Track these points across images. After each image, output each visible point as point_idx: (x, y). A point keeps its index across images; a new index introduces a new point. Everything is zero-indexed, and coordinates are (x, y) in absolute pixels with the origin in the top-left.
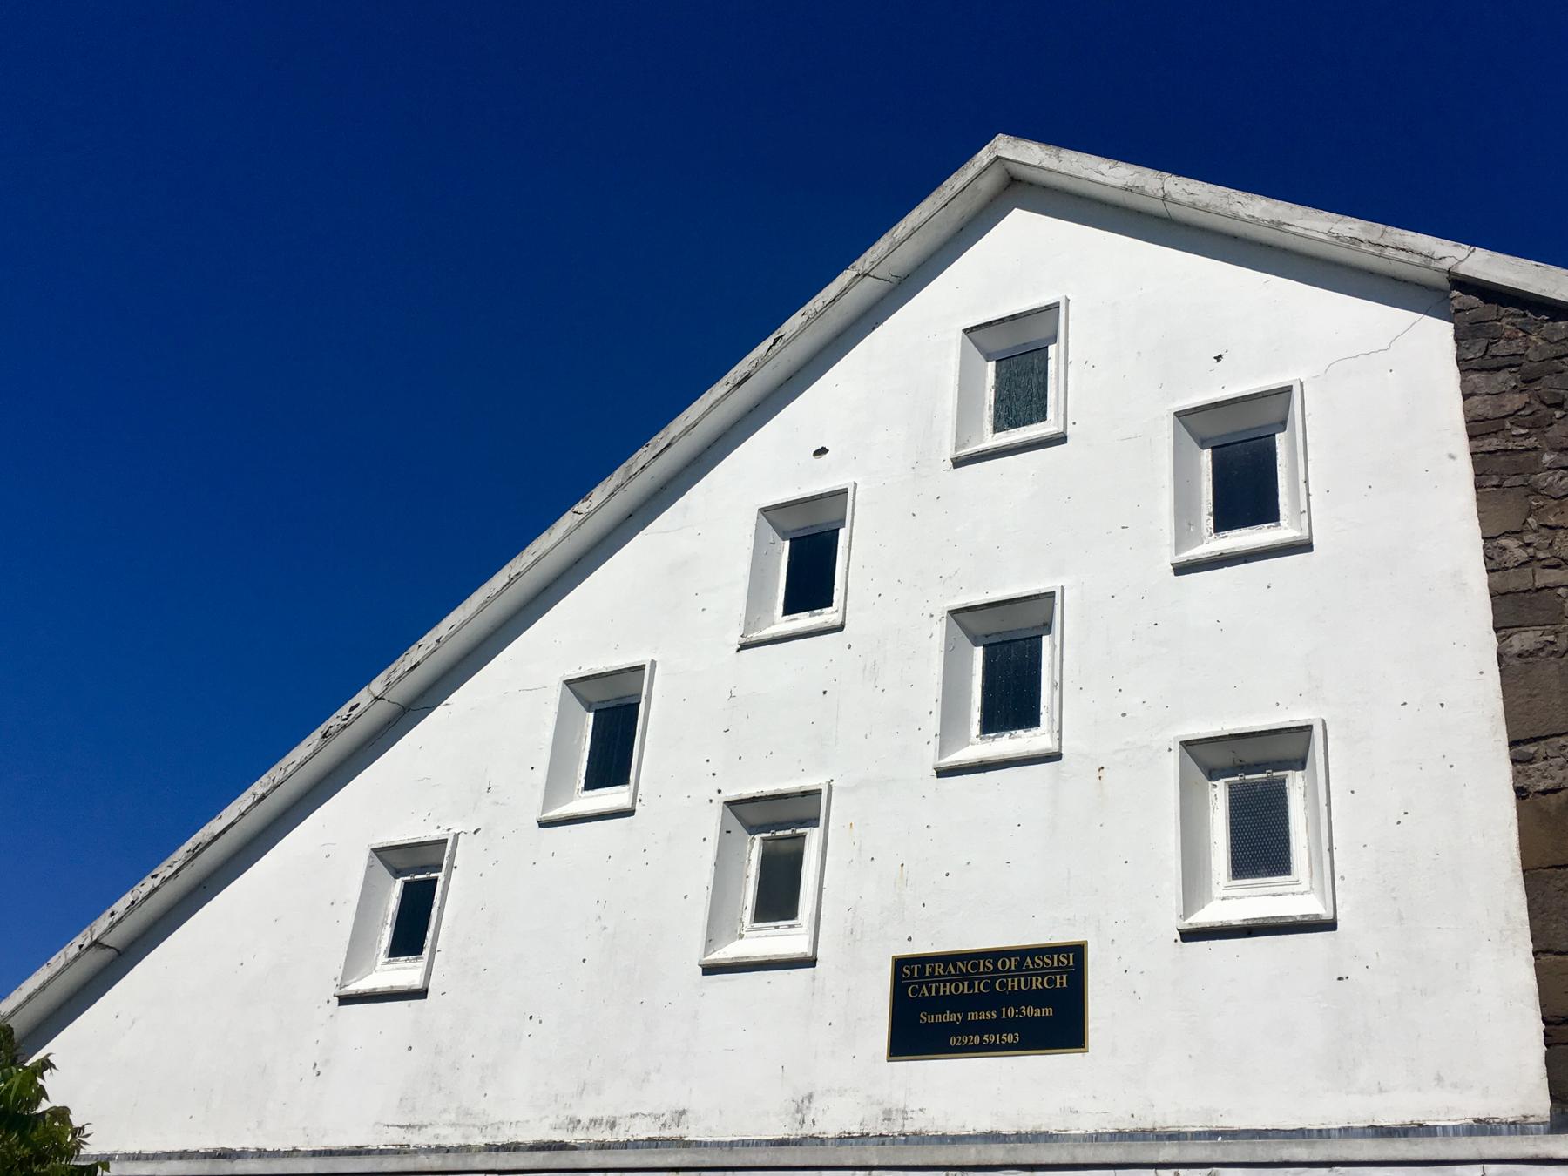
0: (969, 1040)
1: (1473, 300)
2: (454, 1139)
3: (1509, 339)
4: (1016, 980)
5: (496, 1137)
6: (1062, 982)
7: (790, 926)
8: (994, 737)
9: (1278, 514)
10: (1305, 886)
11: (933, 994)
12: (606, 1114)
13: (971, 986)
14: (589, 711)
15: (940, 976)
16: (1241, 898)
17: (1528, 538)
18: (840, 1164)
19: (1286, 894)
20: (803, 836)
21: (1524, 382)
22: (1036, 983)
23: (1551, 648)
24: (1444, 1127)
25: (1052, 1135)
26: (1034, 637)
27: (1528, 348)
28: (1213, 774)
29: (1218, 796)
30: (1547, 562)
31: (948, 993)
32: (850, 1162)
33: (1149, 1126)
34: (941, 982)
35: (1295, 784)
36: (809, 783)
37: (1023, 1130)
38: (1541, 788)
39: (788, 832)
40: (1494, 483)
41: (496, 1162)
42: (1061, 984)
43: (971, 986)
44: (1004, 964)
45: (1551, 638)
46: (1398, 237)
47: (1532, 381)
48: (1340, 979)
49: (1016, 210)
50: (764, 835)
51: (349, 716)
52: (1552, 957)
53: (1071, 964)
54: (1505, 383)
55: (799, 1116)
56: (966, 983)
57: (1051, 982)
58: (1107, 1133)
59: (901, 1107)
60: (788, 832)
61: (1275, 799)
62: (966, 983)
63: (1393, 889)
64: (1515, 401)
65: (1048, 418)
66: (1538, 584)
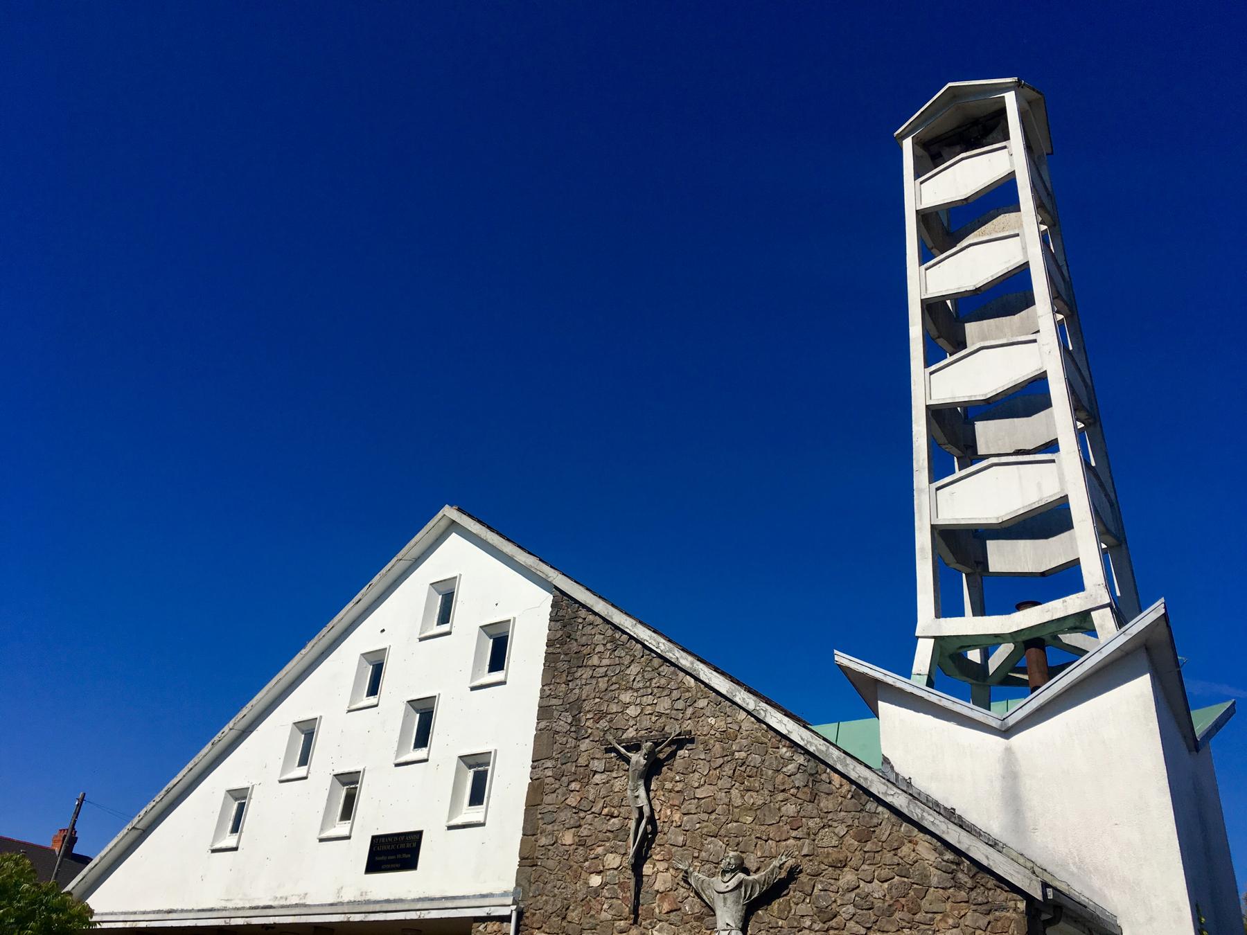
6: (414, 845)
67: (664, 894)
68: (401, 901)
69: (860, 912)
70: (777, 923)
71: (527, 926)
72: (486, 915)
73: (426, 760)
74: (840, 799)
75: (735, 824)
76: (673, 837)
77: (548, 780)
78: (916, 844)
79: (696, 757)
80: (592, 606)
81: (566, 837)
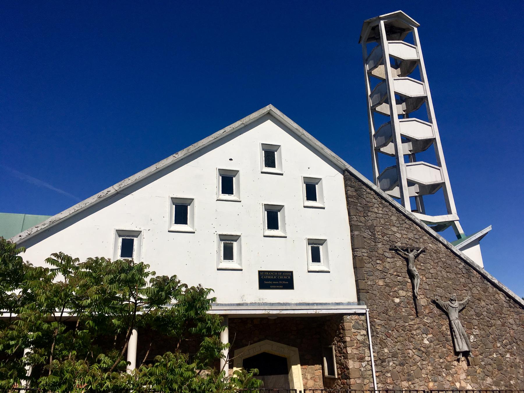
1: (349, 174)
3: (353, 183)
6: (289, 277)
7: (232, 261)
10: (323, 265)
13: (273, 277)
17: (357, 217)
20: (233, 243)
22: (285, 277)
33: (304, 302)
35: (235, 245)
43: (273, 277)
44: (279, 274)
49: (269, 120)
50: (224, 242)
51: (107, 194)
52: (360, 280)
59: (262, 298)
61: (318, 249)
64: (355, 194)
66: (358, 225)
67: (425, 307)
68: (289, 304)
69: (488, 314)
70: (465, 317)
72: (353, 312)
74: (477, 279)
75: (446, 284)
76: (425, 286)
78: (499, 294)
79: (428, 258)
81: (380, 282)
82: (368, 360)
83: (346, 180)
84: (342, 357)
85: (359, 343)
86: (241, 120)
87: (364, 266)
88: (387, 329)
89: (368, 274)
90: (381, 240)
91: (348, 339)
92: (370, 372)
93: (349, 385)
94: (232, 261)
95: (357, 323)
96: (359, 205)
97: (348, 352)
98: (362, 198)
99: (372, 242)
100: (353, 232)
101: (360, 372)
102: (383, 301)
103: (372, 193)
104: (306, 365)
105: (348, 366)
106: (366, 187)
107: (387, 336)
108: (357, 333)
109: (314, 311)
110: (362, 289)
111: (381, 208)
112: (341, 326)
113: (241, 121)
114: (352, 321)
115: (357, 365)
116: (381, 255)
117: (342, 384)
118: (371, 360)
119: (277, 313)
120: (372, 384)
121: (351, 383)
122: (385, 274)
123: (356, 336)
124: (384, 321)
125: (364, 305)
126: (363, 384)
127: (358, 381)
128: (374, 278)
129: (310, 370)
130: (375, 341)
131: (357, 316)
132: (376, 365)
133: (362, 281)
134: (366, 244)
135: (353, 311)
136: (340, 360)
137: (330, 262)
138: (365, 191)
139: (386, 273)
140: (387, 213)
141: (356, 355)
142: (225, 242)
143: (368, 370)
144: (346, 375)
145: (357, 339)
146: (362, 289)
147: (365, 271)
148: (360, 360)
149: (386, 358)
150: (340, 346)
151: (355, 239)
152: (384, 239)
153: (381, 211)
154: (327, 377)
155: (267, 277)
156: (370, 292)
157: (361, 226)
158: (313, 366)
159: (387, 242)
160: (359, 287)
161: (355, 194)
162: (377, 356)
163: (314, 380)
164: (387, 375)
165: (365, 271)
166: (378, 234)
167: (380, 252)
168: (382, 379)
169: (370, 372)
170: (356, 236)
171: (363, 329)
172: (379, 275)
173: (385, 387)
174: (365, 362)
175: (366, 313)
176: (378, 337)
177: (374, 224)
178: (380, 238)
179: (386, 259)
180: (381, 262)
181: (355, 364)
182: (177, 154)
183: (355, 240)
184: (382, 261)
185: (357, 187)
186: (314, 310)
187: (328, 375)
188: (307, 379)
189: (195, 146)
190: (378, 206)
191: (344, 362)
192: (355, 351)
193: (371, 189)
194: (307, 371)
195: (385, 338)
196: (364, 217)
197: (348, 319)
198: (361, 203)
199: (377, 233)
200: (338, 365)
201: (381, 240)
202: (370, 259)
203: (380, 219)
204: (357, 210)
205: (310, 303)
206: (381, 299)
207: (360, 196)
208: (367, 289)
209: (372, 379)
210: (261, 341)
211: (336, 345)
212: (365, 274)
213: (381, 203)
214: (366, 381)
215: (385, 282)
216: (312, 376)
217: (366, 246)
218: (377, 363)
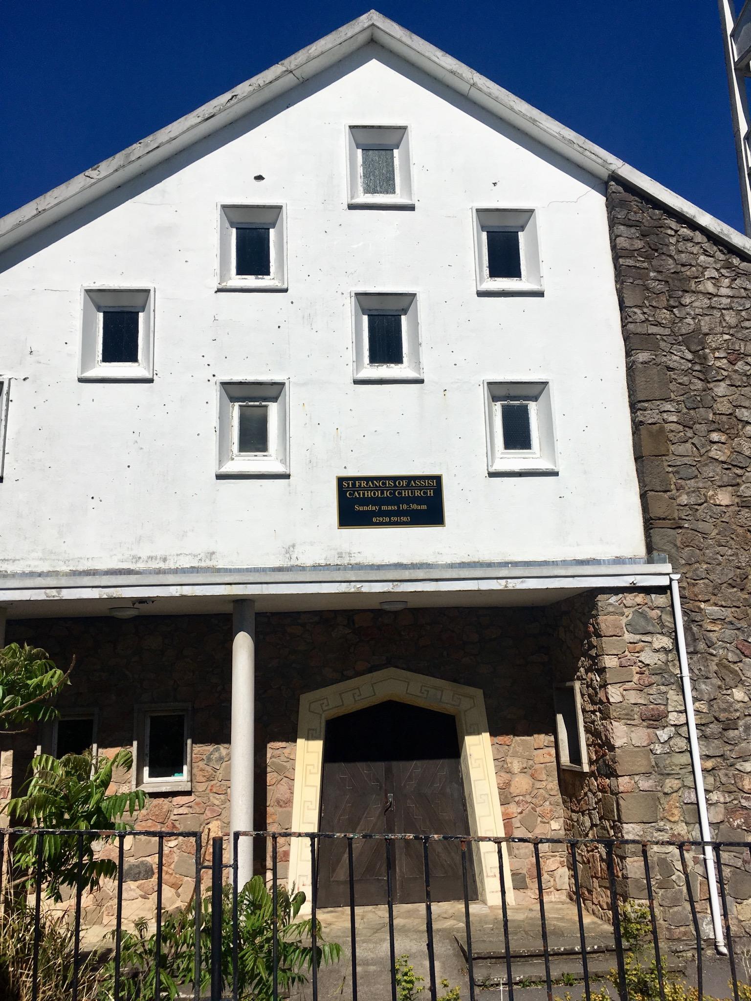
0: (383, 519)
1: (620, 189)
2: (45, 567)
3: (635, 213)
4: (407, 491)
5: (77, 566)
6: (431, 493)
7: (264, 456)
8: (377, 366)
9: (521, 274)
10: (538, 455)
11: (361, 496)
12: (160, 553)
13: (382, 493)
14: (99, 311)
15: (364, 487)
16: (509, 458)
17: (645, 310)
18: (334, 580)
19: (530, 458)
20: (266, 406)
21: (642, 235)
22: (417, 493)
23: (654, 362)
24: (604, 560)
25: (429, 564)
26: (397, 315)
27: (643, 219)
28: (233, 399)
29: (235, 411)
30: (652, 323)
31: (369, 496)
32: (339, 579)
33: (477, 560)
34: (366, 490)
35: (273, 410)
36: (277, 378)
37: (415, 562)
38: (650, 422)
39: (257, 403)
40: (631, 281)
41: (100, 581)
42: (430, 494)
43: (382, 493)
44: (399, 483)
45: (654, 357)
46: (591, 146)
47: (646, 236)
48: (560, 497)
52: (654, 493)
53: (435, 485)
54: (634, 233)
55: (288, 555)
56: (379, 492)
57: (425, 493)
58: (456, 563)
60: (257, 403)
61: (524, 413)
62: (379, 492)
63: (582, 460)
64: (639, 244)
65: (397, 193)
66: (650, 332)
71: (686, 598)
73: (151, 381)
77: (668, 427)
80: (694, 217)
81: (720, 496)
82: (676, 722)
83: (611, 206)
84: (598, 714)
85: (647, 672)
86: (283, 61)
87: (668, 451)
88: (743, 632)
89: (681, 472)
90: (725, 373)
91: (610, 662)
92: (684, 759)
93: (617, 794)
94: (264, 456)
95: (643, 615)
96: (652, 274)
97: (612, 700)
98: (663, 253)
99: (696, 381)
100: (632, 356)
101: (652, 757)
102: (730, 552)
103: (699, 237)
104: (507, 734)
105: (612, 740)
106: (677, 222)
107: (743, 653)
108: (642, 643)
109: (500, 584)
110: (660, 519)
111: (727, 280)
112: (593, 624)
113: (282, 64)
114: (625, 610)
115: (640, 736)
116: (724, 418)
117: (600, 790)
118: (687, 724)
119: (385, 590)
120: (689, 793)
121: (621, 789)
122: (739, 472)
123: (638, 652)
124: (733, 609)
125: (665, 562)
126: (659, 791)
127: (645, 784)
128: (701, 485)
129: (520, 749)
130: (703, 668)
131: (642, 595)
132: (703, 737)
133: (660, 493)
134: (672, 386)
135: (626, 582)
136: (593, 722)
137: (559, 446)
138: (673, 233)
139: (742, 468)
140: (747, 292)
141: (636, 709)
142: (245, 404)
143: (678, 750)
144: (608, 766)
145: (640, 661)
146: (660, 519)
147: (669, 466)
148: (652, 722)
149: (738, 718)
150: (591, 683)
151: (637, 373)
152: (736, 371)
153: (728, 287)
154: (564, 768)
155: (364, 494)
156: (686, 525)
157: (658, 337)
158: (529, 738)
159: (745, 378)
160: (649, 514)
161: (639, 244)
162: (709, 710)
163: (532, 776)
164: (741, 768)
165: (669, 466)
166: (717, 355)
167: (723, 407)
168: (724, 780)
169: (684, 759)
170: (640, 366)
171: (662, 634)
172: (717, 475)
173: (735, 802)
174: (666, 730)
175: (669, 587)
176: (712, 655)
177: (703, 328)
178: (723, 369)
179: (744, 427)
180: (723, 438)
181: (633, 735)
182: (95, 169)
183: (637, 378)
184: (727, 434)
185: (646, 224)
186: (499, 581)
187: (569, 764)
188: (509, 772)
189: (147, 145)
190: (715, 274)
191: (602, 727)
192: (633, 697)
193: (693, 225)
194: (510, 752)
195: (736, 659)
196: (670, 308)
197: (611, 604)
198: (660, 270)
199: (714, 354)
200: (588, 735)
201: (725, 373)
202: (687, 429)
203: (723, 311)
204: (648, 289)
205: (494, 563)
206: (724, 544)
207: (656, 251)
208: (676, 515)
209: (692, 777)
210: (375, 671)
211: (585, 679)
212: (671, 475)
213: (729, 266)
214: (671, 784)
215: (738, 496)
216: (525, 766)
217: (673, 392)
218: (708, 731)
